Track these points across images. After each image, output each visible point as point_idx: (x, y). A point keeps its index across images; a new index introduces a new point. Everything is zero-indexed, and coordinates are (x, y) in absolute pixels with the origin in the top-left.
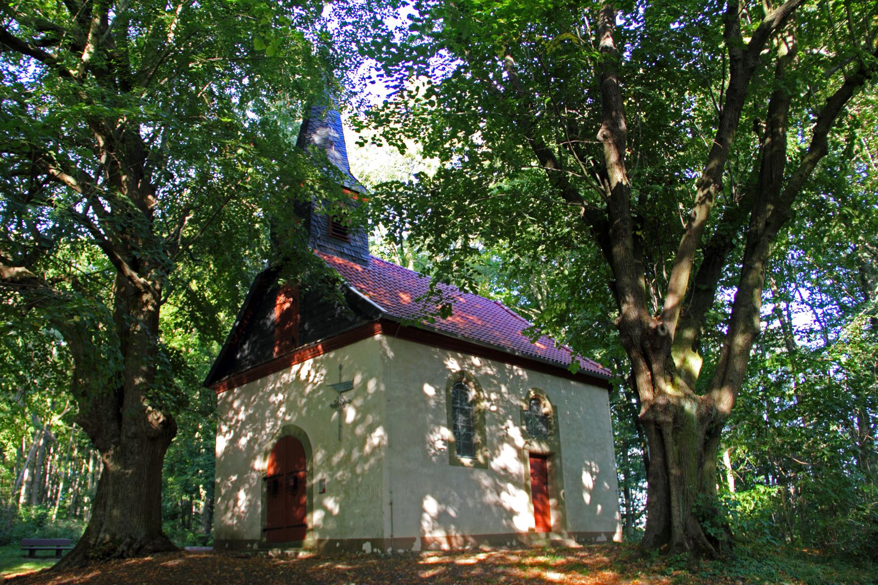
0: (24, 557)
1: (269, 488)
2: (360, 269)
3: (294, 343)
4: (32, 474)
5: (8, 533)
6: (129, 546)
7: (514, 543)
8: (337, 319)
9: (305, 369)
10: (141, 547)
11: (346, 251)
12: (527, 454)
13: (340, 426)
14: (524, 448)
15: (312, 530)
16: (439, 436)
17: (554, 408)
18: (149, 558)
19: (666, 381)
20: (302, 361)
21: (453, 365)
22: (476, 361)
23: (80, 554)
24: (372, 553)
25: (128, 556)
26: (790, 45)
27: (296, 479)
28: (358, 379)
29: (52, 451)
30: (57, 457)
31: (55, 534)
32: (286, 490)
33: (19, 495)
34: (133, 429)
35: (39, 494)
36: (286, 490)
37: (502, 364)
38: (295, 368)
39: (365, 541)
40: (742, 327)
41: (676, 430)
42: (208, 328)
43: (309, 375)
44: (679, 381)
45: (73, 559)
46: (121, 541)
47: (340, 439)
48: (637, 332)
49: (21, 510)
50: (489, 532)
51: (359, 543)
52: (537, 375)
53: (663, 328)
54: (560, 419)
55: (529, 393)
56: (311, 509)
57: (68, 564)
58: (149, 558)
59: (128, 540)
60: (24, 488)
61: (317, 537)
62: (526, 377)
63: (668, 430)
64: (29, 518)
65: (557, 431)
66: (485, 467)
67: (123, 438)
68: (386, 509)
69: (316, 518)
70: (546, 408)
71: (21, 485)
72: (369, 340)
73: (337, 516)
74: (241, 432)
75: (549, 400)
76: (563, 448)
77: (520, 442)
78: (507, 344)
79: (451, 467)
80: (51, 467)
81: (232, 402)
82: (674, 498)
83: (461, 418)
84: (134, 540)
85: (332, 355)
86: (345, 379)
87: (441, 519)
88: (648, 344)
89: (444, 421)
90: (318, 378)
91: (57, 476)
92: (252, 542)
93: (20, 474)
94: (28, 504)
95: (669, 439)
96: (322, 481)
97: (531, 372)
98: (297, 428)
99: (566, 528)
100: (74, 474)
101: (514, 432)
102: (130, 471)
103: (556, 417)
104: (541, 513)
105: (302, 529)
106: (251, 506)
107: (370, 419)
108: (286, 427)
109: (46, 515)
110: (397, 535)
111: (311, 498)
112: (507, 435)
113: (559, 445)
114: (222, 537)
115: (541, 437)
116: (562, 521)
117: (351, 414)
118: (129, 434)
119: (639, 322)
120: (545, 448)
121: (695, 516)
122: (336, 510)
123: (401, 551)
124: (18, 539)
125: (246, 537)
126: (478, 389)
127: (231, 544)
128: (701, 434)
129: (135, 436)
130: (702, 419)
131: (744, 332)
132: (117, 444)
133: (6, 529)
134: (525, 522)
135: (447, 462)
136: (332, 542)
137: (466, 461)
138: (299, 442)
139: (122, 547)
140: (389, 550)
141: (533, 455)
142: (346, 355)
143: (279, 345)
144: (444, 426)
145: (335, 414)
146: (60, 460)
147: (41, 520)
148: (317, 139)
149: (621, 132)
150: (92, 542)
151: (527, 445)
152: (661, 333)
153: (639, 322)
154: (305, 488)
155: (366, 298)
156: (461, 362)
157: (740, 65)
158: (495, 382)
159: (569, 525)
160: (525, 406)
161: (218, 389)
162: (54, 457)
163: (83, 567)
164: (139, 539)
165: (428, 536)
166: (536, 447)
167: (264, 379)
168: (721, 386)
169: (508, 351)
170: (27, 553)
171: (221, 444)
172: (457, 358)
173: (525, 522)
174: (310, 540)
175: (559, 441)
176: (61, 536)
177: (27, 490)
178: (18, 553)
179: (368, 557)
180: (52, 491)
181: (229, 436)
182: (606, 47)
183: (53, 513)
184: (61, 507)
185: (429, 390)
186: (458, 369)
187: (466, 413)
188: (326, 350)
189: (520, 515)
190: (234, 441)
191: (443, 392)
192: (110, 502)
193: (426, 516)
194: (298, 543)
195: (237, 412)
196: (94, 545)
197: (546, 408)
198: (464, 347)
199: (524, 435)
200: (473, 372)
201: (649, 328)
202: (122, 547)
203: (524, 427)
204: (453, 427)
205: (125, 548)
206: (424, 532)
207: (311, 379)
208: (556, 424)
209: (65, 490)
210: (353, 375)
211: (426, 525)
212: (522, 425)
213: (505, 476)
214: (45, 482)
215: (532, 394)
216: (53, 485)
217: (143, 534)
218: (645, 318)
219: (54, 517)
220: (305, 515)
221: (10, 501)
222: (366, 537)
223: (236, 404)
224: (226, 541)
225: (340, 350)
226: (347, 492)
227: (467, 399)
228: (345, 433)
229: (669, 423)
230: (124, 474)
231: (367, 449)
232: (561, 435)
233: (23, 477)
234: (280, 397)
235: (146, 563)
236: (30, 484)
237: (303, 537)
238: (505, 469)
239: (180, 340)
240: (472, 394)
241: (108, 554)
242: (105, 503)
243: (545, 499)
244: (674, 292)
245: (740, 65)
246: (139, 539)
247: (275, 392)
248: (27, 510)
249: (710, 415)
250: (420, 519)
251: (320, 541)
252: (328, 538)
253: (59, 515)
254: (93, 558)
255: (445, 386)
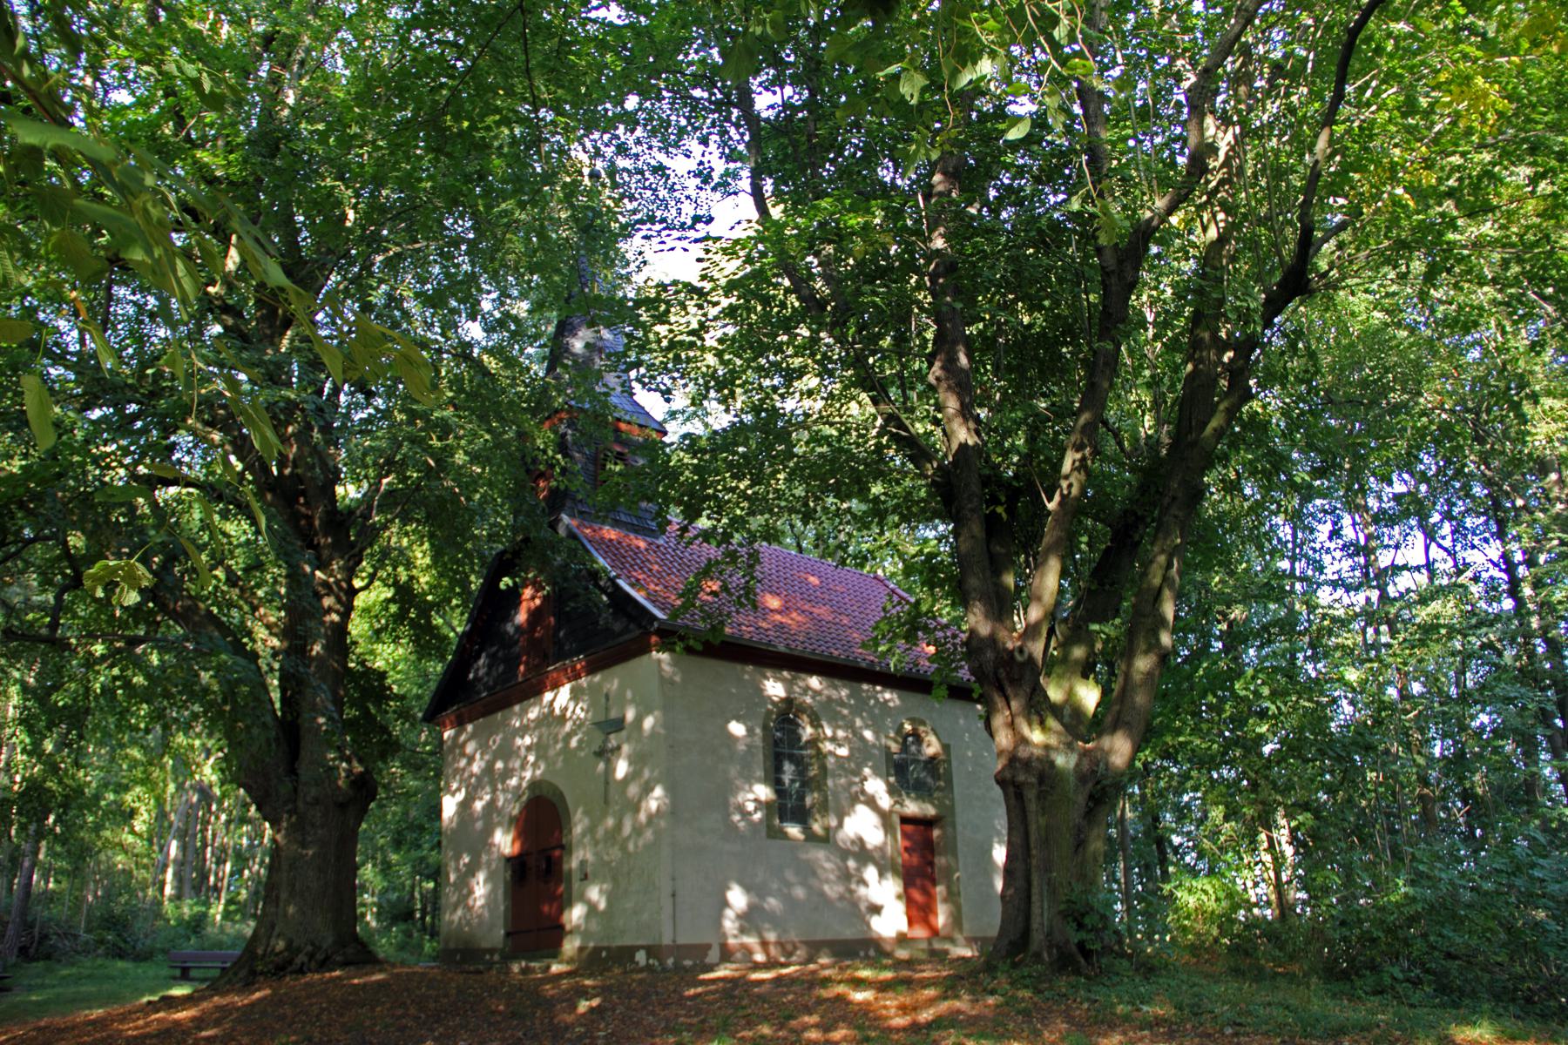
0: (175, 978)
1: (514, 872)
2: (642, 545)
3: (546, 659)
4: (184, 848)
5: (148, 942)
6: (311, 956)
7: (872, 953)
8: (599, 630)
9: (561, 698)
10: (327, 958)
11: (623, 518)
12: (896, 820)
13: (607, 783)
14: (891, 812)
15: (571, 932)
16: (751, 796)
17: (946, 748)
18: (338, 973)
19: (1030, 725)
20: (556, 686)
21: (775, 689)
22: (814, 682)
23: (248, 966)
24: (648, 965)
25: (310, 970)
26: (1222, 225)
27: (549, 860)
28: (630, 715)
29: (214, 807)
30: (224, 817)
31: (220, 945)
32: (538, 875)
33: (163, 883)
34: (313, 792)
35: (196, 883)
36: (538, 875)
37: (855, 685)
38: (548, 696)
39: (638, 948)
40: (1143, 647)
41: (1041, 796)
42: (426, 640)
43: (566, 709)
44: (1052, 722)
45: (235, 974)
46: (299, 950)
47: (606, 801)
48: (989, 655)
49: (168, 907)
50: (829, 936)
51: (632, 950)
52: (915, 699)
53: (1021, 650)
54: (954, 764)
55: (902, 725)
56: (568, 903)
57: (229, 982)
58: (338, 973)
59: (310, 948)
60: (170, 871)
61: (577, 943)
62: (898, 702)
63: (1031, 794)
64: (180, 920)
65: (949, 782)
66: (827, 839)
67: (301, 805)
68: (667, 902)
69: (576, 914)
70: (932, 747)
71: (165, 866)
72: (645, 658)
73: (604, 913)
74: (478, 786)
75: (936, 734)
76: (958, 809)
77: (885, 802)
78: (863, 656)
79: (770, 842)
80: (214, 836)
81: (465, 743)
82: (1035, 890)
83: (788, 767)
84: (317, 948)
85: (597, 678)
86: (613, 714)
87: (749, 920)
88: (1002, 673)
89: (760, 773)
90: (579, 711)
91: (223, 848)
92: (492, 951)
93: (163, 848)
94: (178, 897)
95: (1032, 807)
96: (583, 863)
97: (905, 694)
98: (551, 784)
99: (961, 930)
100: (251, 846)
101: (876, 786)
102: (310, 852)
103: (949, 762)
104: (919, 911)
105: (557, 931)
106: (491, 897)
107: (646, 774)
108: (534, 784)
109: (204, 915)
110: (681, 941)
111: (569, 887)
112: (863, 792)
113: (952, 808)
114: (452, 945)
115: (920, 790)
116: (956, 920)
117: (622, 769)
118: (309, 799)
119: (992, 640)
120: (931, 811)
121: (1065, 915)
122: (602, 905)
123: (688, 963)
124: (164, 951)
125: (485, 945)
126: (816, 724)
127: (463, 955)
128: (1081, 799)
129: (317, 801)
130: (1082, 777)
131: (1146, 652)
132: (290, 813)
133: (146, 936)
134: (891, 921)
135: (764, 834)
136: (597, 950)
137: (794, 831)
138: (554, 805)
139: (301, 959)
140: (670, 961)
141: (905, 820)
142: (610, 681)
143: (526, 664)
144: (759, 781)
145: (601, 766)
146: (228, 822)
147: (198, 923)
148: (578, 345)
149: (962, 370)
150: (260, 951)
151: (897, 807)
152: (1019, 658)
153: (992, 640)
154: (561, 870)
155: (639, 596)
156: (789, 684)
157: (1114, 280)
158: (845, 712)
159: (966, 926)
160: (894, 747)
161: (444, 725)
162: (218, 818)
163: (248, 985)
164: (325, 946)
165: (731, 941)
166: (912, 808)
167: (506, 711)
168: (1114, 729)
169: (864, 665)
170: (178, 972)
171: (450, 806)
172: (783, 680)
173: (891, 921)
174: (570, 946)
175: (952, 800)
176: (228, 948)
177: (175, 874)
178: (165, 972)
179: (641, 970)
180: (216, 875)
181: (460, 796)
182: (938, 250)
183: (217, 910)
184: (230, 902)
185: (737, 729)
186: (783, 694)
187: (799, 762)
188: (592, 669)
189: (884, 912)
190: (465, 806)
191: (758, 731)
192: (284, 896)
193: (729, 913)
194: (554, 950)
195: (471, 759)
196: (264, 955)
197: (932, 747)
198: (795, 663)
199: (891, 791)
200: (808, 700)
201: (1006, 649)
202: (301, 959)
203: (892, 779)
204: (776, 783)
205: (305, 959)
206: (724, 936)
207: (568, 714)
208: (949, 772)
209: (237, 872)
210: (623, 709)
211: (729, 924)
212: (888, 775)
213: (863, 853)
214: (205, 860)
215: (908, 727)
216: (218, 863)
217: (330, 940)
218: (1002, 634)
219: (219, 917)
220: (561, 912)
221: (150, 892)
222: (640, 943)
223: (470, 748)
224: (457, 951)
225: (606, 672)
226: (615, 876)
227: (799, 739)
228: (614, 795)
229: (1032, 784)
230: (302, 856)
231: (642, 817)
232: (956, 790)
233: (168, 853)
234: (528, 740)
235: (332, 979)
236: (180, 864)
237: (558, 944)
238: (860, 841)
239: (389, 656)
240: (808, 732)
241: (281, 968)
242: (278, 897)
243: (929, 885)
244: (1039, 599)
245: (1114, 280)
246: (325, 946)
247: (523, 731)
248: (178, 908)
249: (1094, 772)
250: (719, 917)
251: (581, 949)
252: (591, 944)
253: (227, 915)
254: (262, 973)
255: (761, 722)
